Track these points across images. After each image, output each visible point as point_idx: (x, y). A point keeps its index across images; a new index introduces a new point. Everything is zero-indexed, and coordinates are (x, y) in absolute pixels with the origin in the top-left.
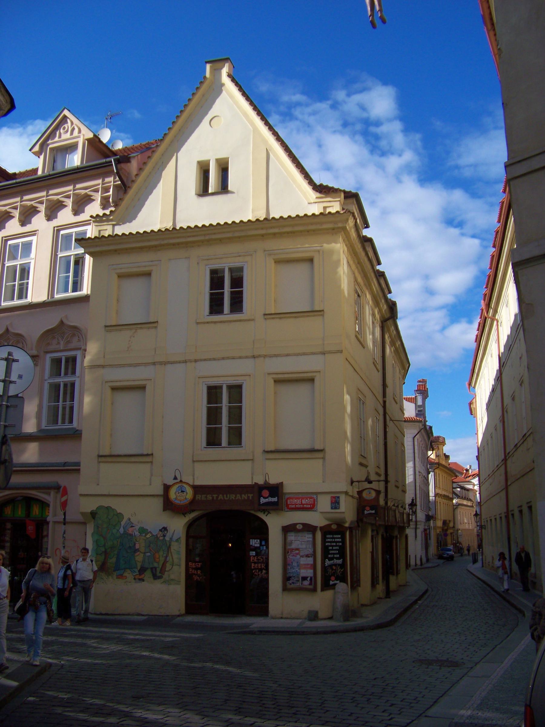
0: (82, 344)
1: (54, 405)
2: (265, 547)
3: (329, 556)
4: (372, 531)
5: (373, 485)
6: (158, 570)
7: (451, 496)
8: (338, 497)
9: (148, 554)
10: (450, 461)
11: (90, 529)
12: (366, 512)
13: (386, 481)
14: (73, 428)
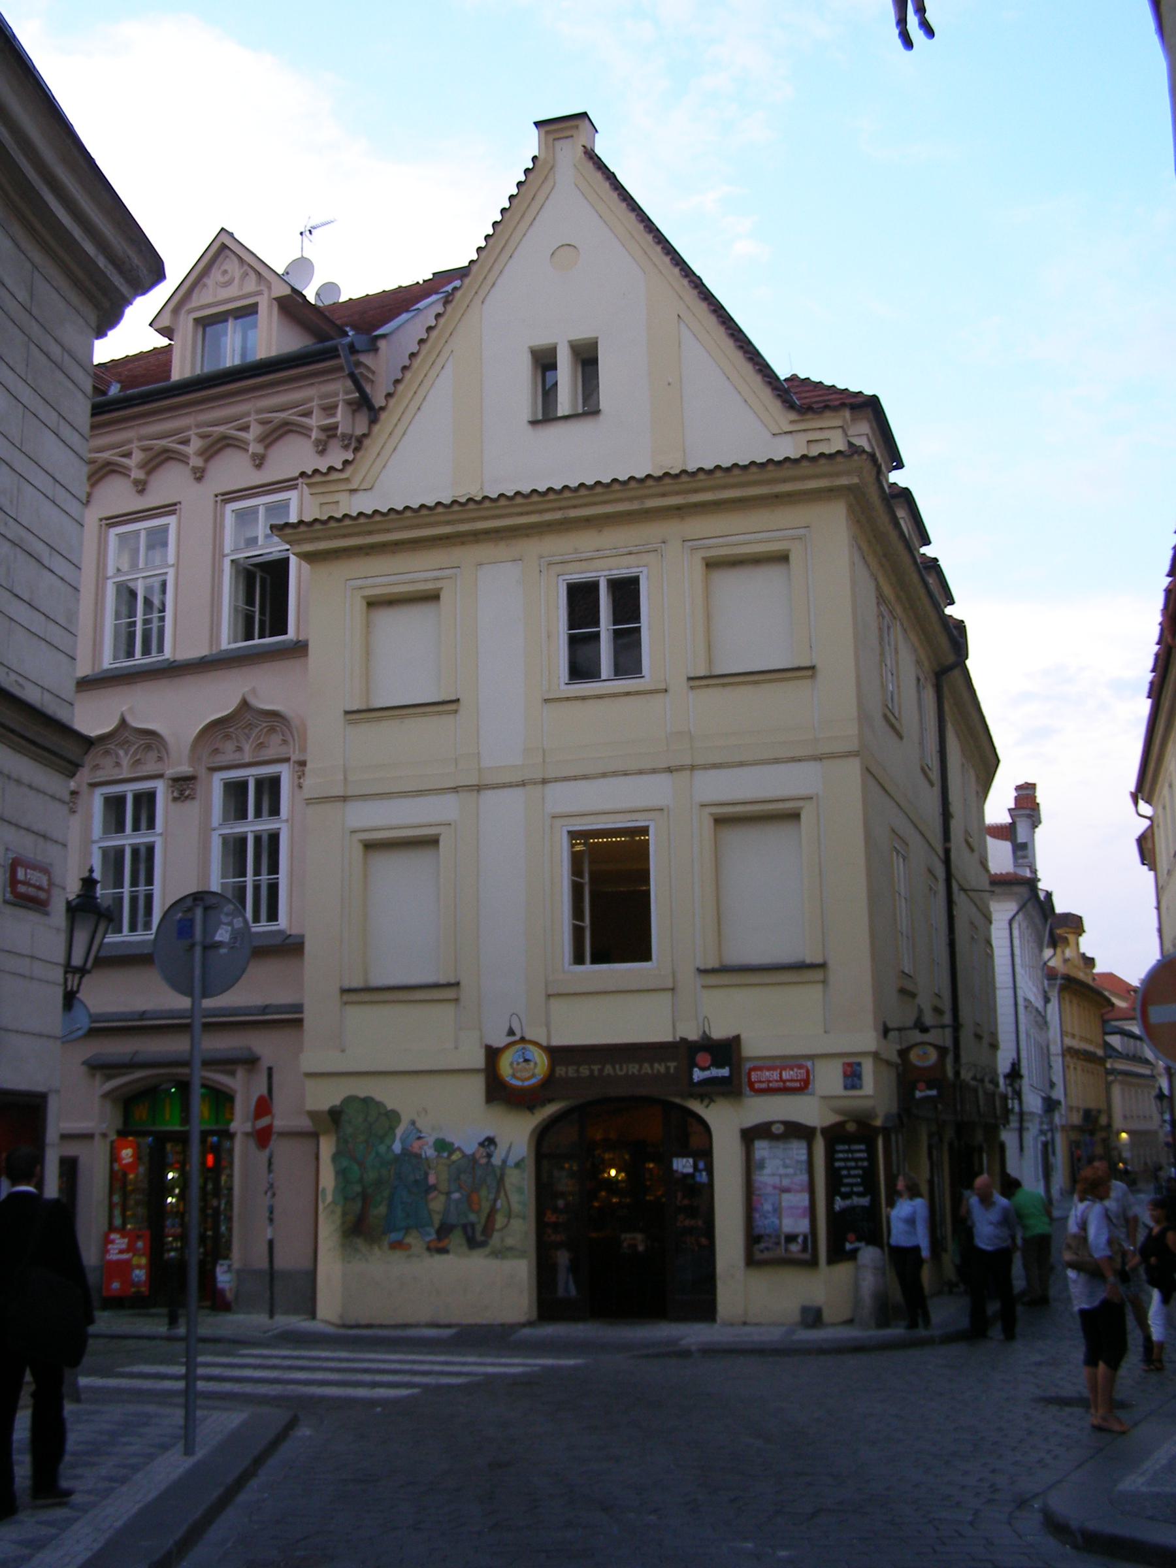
0: (292, 750)
1: (234, 882)
2: (704, 1173)
3: (843, 1189)
4: (931, 1135)
5: (931, 1037)
6: (479, 1228)
7: (1100, 1052)
8: (859, 1064)
9: (456, 1196)
10: (1096, 971)
11: (327, 1146)
12: (918, 1094)
13: (956, 1027)
14: (280, 932)
